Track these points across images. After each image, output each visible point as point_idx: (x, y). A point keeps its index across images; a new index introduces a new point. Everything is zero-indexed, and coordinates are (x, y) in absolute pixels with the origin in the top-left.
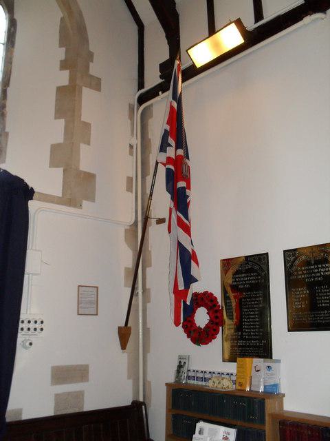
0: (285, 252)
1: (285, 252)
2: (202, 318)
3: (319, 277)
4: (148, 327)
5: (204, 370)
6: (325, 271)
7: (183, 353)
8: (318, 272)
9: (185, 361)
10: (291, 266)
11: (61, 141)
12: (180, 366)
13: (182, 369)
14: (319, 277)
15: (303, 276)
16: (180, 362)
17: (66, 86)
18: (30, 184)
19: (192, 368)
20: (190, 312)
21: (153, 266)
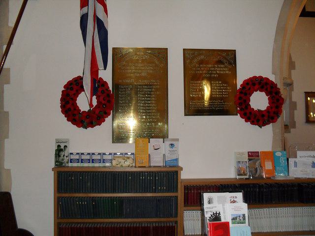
0: (235, 51)
1: (235, 51)
2: (84, 102)
3: (215, 74)
4: (6, 109)
5: (91, 151)
6: (220, 71)
7: (62, 137)
8: (214, 70)
9: (65, 144)
10: (191, 63)
11: (5, 85)
12: (59, 151)
13: (62, 154)
14: (215, 74)
15: (201, 72)
16: (59, 146)
17: (3, 109)
18: (61, 93)
19: (74, 151)
20: (98, 119)
21: (297, 128)
